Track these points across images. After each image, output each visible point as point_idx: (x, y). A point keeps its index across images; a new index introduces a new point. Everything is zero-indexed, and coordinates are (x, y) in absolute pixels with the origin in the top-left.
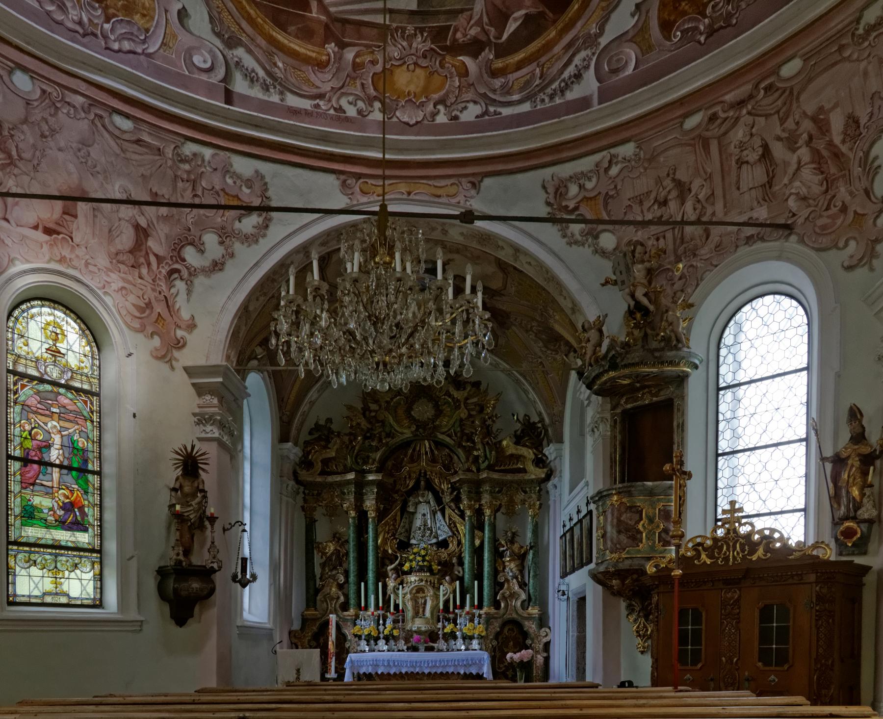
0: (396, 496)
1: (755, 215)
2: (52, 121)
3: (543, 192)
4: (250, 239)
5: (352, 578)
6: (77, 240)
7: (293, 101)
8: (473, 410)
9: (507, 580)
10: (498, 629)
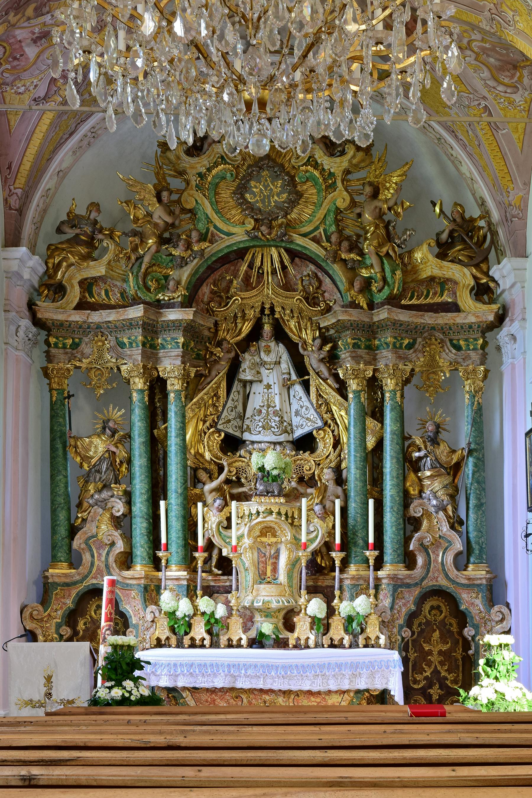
9: (427, 514)
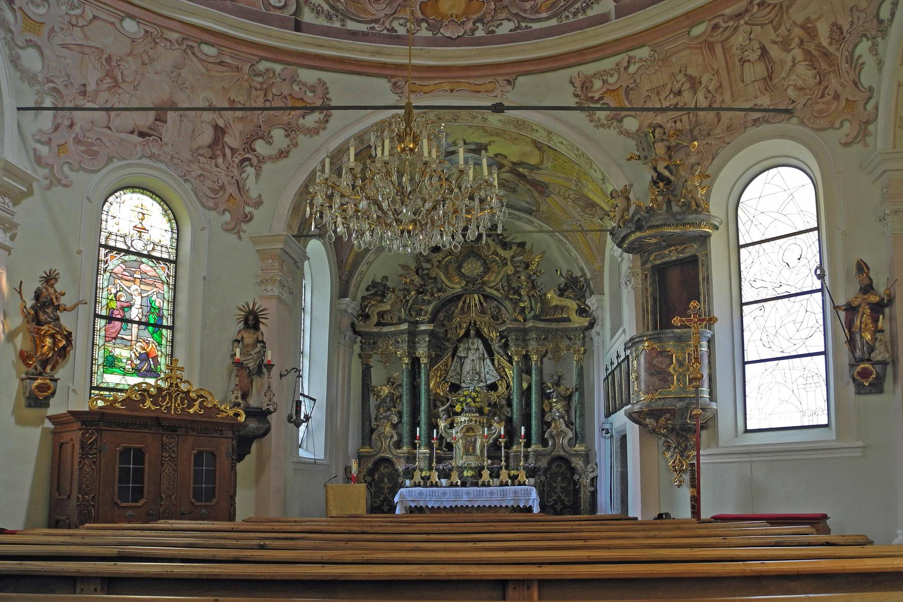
0: (447, 344)
1: (759, 102)
2: (151, 52)
3: (571, 86)
4: (313, 132)
5: (405, 419)
6: (165, 140)
7: (351, 25)
8: (518, 267)
9: (553, 419)
10: (546, 466)
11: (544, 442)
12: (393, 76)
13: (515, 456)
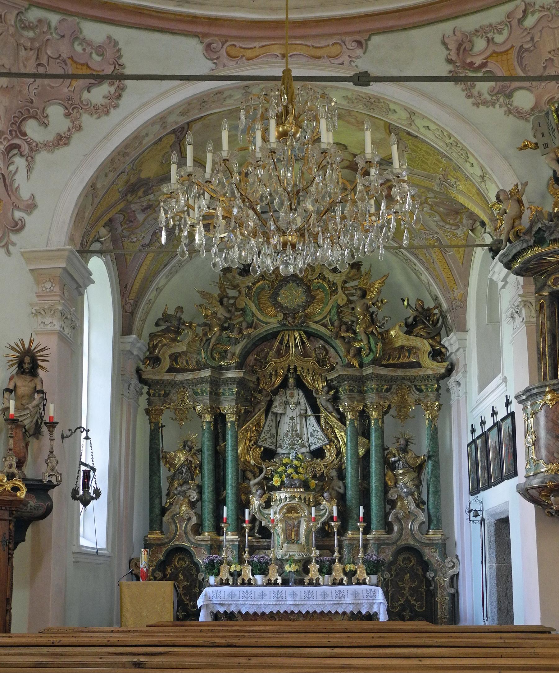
0: (259, 396)
3: (443, 48)
5: (208, 495)
8: (352, 295)
9: (400, 497)
10: (391, 559)
11: (388, 528)
12: (206, 35)
13: (351, 544)
